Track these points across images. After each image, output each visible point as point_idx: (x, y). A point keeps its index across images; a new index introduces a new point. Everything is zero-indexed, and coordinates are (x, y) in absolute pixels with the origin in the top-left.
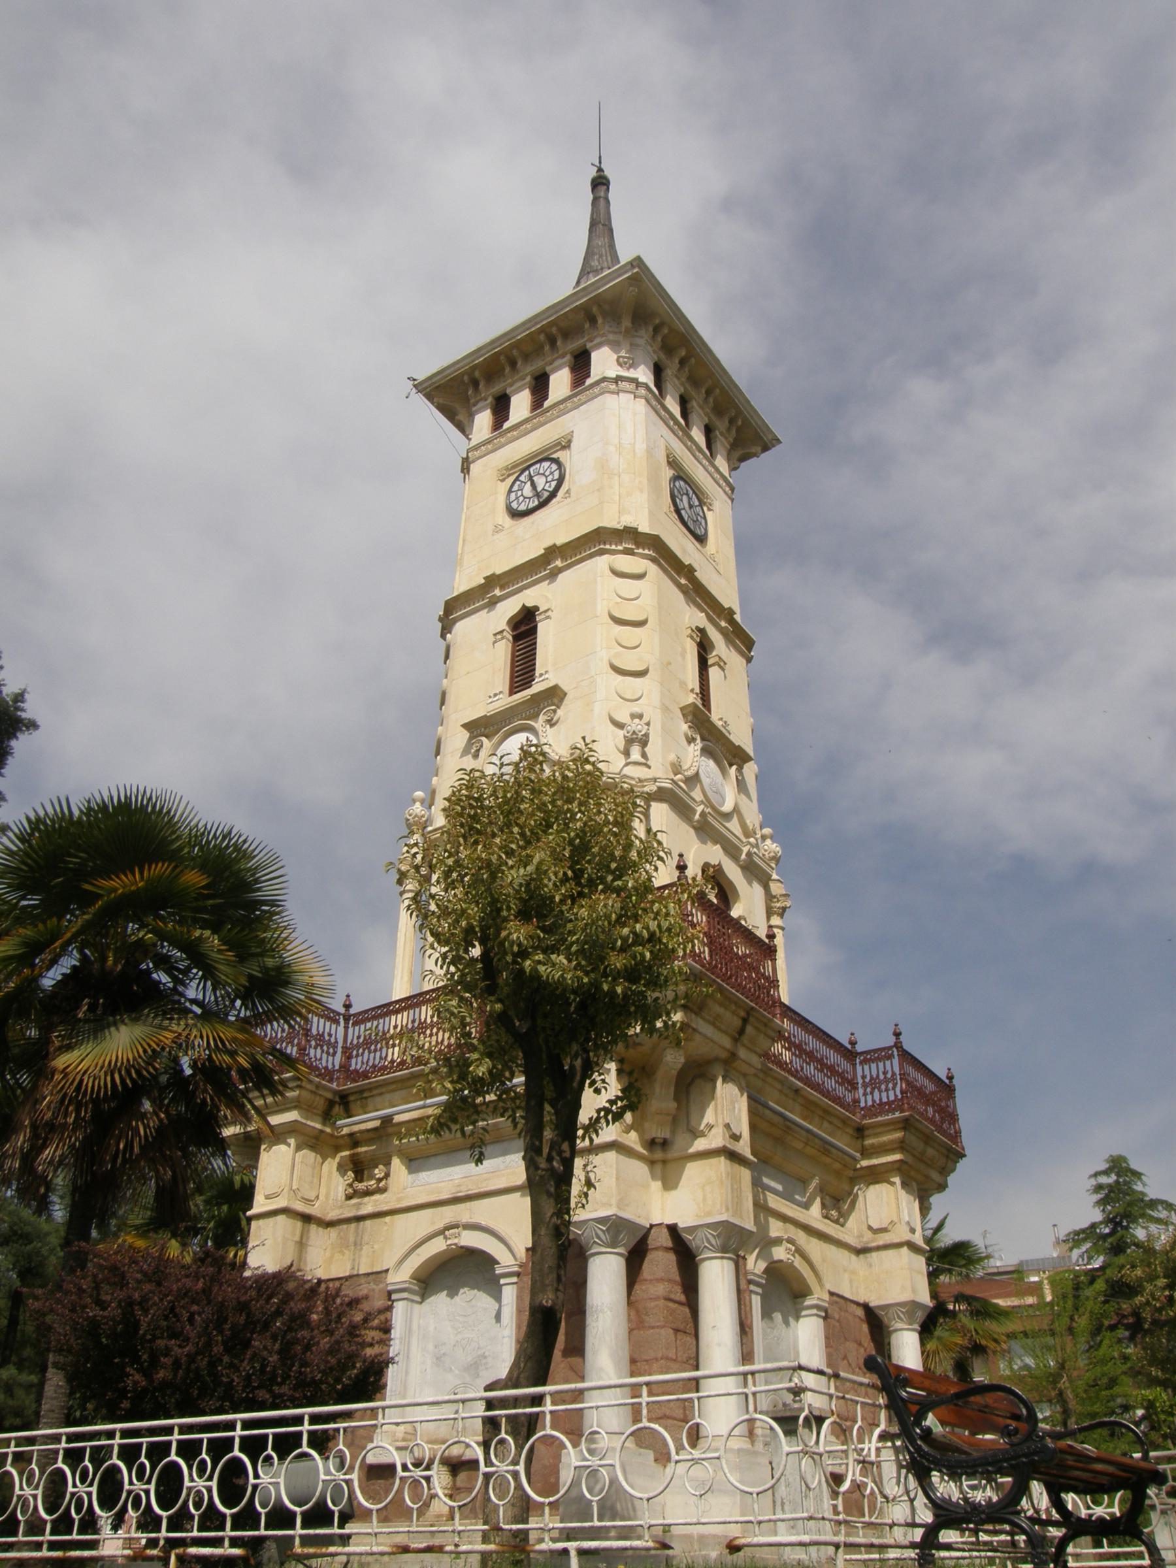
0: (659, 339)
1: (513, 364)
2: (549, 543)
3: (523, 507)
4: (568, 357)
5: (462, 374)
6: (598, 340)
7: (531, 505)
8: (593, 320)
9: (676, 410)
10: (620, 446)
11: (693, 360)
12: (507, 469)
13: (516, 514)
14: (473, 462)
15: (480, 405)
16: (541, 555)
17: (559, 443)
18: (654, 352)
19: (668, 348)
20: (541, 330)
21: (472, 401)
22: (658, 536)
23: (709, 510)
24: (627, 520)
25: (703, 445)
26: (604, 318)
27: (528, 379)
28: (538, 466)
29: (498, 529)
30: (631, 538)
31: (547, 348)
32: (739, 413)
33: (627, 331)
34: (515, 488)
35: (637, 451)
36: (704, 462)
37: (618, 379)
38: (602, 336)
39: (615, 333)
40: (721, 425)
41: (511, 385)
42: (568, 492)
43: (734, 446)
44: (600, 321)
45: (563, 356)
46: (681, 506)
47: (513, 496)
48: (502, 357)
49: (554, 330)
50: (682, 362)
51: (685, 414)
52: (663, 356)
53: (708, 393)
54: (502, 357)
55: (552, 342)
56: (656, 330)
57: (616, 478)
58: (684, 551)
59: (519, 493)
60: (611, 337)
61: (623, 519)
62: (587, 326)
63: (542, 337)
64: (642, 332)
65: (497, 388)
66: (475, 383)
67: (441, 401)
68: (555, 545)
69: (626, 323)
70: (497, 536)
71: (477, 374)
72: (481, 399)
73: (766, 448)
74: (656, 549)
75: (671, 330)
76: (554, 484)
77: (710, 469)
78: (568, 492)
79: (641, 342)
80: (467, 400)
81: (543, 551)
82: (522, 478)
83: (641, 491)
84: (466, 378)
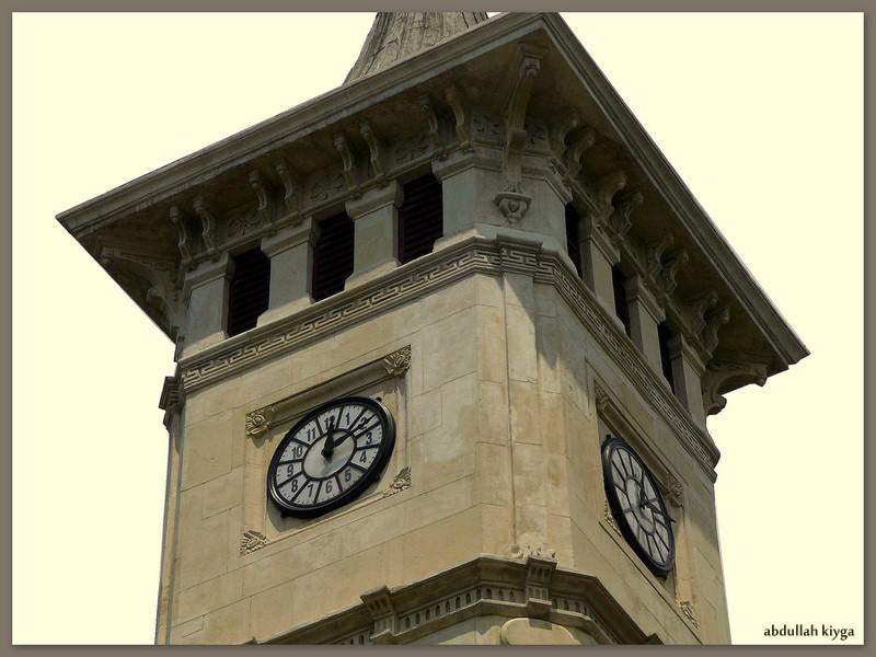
0: (577, 158)
1: (275, 190)
2: (371, 587)
3: (305, 499)
4: (392, 188)
5: (167, 204)
6: (457, 158)
7: (324, 497)
8: (445, 117)
9: (605, 298)
10: (509, 387)
11: (640, 198)
12: (266, 411)
13: (291, 514)
14: (195, 391)
15: (205, 268)
16: (356, 609)
17: (382, 368)
18: (567, 183)
19: (591, 177)
20: (339, 128)
21: (186, 260)
22: (595, 580)
23: (676, 506)
24: (529, 547)
25: (611, 311)
26: (467, 112)
27: (308, 224)
28: (335, 412)
29: (251, 541)
30: (540, 573)
31: (348, 166)
32: (726, 298)
33: (517, 143)
34: (288, 455)
35: (545, 396)
36: (663, 405)
37: (497, 247)
38: (465, 150)
39: (492, 145)
40: (690, 323)
41: (271, 234)
42: (405, 473)
43: (713, 365)
44: (460, 120)
45: (382, 184)
46: (624, 505)
47: (282, 474)
48: (253, 177)
49: (365, 130)
50: (619, 201)
51: (623, 309)
52: (582, 190)
53: (667, 260)
54: (253, 177)
55: (360, 153)
56: (572, 139)
57: (505, 452)
58: (637, 602)
59: (297, 468)
60: (483, 153)
61: (521, 542)
62: (434, 129)
63: (339, 143)
64: (544, 145)
65: (240, 238)
66: (193, 225)
67: (118, 254)
68: (385, 590)
69: (514, 127)
70: (250, 558)
71: (198, 206)
72: (207, 258)
73: (777, 367)
74: (595, 613)
75: (600, 140)
76: (372, 454)
77: (675, 420)
78: (405, 473)
79: (540, 163)
80: (176, 256)
81: (359, 602)
82: (302, 435)
83: (555, 479)
84: (174, 212)
